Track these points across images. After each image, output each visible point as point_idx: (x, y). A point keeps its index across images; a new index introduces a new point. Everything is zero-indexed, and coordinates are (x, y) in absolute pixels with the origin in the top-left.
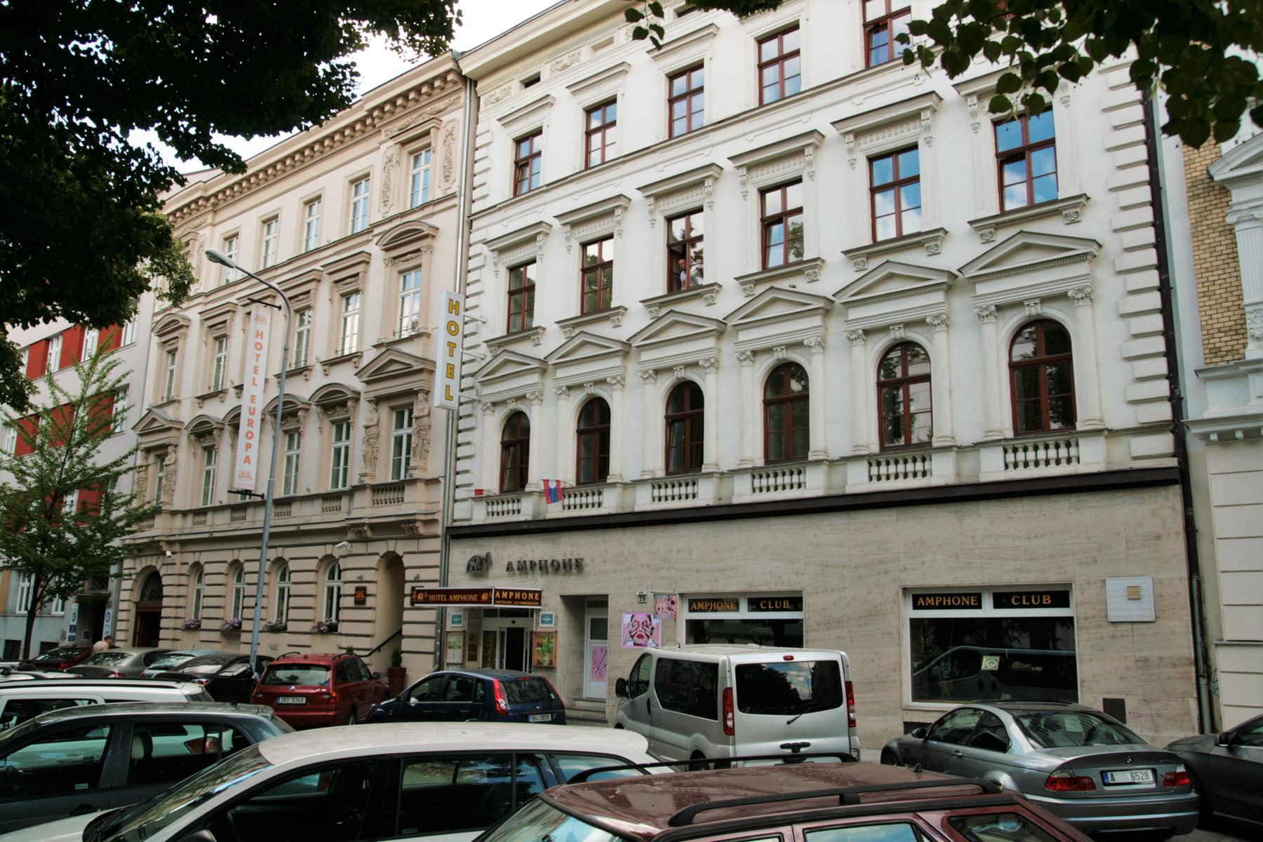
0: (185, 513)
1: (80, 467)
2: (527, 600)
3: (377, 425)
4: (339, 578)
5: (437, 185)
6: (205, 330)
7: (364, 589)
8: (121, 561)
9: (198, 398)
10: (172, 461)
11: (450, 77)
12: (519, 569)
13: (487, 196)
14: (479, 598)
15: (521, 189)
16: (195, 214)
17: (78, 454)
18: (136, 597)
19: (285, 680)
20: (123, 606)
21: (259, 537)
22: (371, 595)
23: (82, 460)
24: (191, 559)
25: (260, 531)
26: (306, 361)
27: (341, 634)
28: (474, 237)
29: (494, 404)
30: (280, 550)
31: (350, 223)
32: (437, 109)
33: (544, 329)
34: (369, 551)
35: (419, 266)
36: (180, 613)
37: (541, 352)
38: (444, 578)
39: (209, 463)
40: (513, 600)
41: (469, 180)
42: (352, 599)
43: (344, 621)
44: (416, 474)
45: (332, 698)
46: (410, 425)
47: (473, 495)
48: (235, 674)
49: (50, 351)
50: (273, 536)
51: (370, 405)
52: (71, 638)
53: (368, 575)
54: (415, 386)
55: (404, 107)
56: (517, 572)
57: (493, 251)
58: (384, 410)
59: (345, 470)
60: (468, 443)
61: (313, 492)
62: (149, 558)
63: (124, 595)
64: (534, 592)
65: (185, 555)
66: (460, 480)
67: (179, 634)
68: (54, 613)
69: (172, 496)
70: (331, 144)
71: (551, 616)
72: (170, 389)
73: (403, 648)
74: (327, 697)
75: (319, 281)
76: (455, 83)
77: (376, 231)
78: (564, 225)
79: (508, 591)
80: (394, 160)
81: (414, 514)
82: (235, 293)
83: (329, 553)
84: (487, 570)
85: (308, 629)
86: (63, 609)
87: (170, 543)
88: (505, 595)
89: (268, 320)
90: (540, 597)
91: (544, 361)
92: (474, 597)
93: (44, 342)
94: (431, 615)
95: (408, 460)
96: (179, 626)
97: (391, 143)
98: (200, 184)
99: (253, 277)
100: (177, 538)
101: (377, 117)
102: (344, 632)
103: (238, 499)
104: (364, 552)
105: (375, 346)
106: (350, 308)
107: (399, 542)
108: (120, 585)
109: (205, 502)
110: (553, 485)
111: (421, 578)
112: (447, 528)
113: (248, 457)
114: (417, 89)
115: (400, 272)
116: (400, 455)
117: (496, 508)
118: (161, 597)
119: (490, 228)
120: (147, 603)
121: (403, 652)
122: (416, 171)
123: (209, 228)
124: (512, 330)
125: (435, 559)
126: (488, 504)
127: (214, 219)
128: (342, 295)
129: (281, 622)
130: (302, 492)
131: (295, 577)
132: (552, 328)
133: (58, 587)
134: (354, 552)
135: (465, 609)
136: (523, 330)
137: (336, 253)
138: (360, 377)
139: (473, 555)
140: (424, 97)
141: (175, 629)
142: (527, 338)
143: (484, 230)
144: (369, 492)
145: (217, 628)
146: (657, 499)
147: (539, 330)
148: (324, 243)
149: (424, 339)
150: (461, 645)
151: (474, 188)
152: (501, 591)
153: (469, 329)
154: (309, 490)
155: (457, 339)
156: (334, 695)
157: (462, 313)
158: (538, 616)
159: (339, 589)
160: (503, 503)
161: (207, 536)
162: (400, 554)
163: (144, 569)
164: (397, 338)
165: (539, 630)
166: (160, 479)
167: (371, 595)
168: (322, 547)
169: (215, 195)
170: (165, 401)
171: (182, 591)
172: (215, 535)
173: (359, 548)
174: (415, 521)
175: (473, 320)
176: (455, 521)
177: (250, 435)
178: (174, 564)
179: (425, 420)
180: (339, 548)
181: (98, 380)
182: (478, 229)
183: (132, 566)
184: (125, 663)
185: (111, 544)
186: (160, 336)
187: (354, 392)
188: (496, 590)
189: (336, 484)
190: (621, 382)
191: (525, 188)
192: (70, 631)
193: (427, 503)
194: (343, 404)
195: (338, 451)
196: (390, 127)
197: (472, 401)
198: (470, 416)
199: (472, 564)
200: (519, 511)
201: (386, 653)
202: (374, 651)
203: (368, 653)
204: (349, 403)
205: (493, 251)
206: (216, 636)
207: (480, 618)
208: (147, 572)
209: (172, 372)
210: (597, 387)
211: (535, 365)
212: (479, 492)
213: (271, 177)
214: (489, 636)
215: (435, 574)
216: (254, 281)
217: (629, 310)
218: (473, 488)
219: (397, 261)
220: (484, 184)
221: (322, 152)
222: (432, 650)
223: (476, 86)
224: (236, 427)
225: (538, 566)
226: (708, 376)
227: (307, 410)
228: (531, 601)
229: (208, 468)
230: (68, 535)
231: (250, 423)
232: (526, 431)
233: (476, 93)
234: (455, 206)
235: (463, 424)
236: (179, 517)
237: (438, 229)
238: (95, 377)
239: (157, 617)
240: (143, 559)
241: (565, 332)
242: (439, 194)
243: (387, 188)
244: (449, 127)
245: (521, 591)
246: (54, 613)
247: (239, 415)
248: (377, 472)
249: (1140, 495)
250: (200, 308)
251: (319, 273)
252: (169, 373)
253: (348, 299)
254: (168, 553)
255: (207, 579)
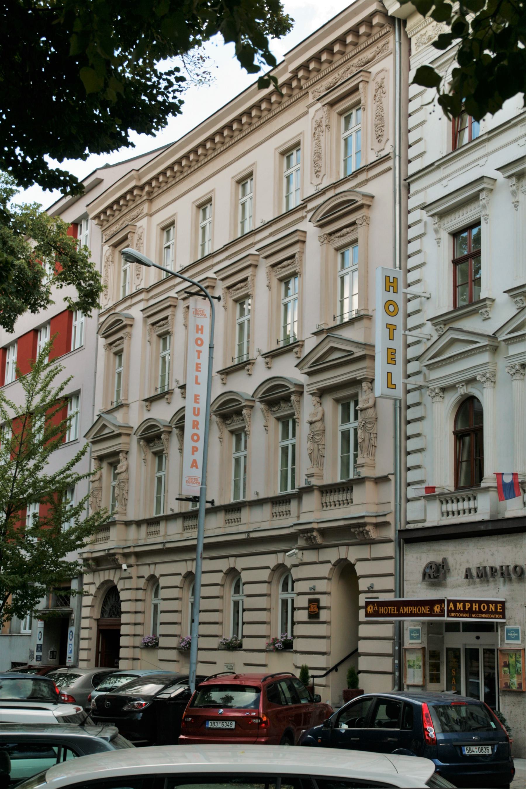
0: (139, 523)
1: (30, 480)
2: (488, 612)
3: (322, 419)
4: (293, 590)
5: (369, 148)
6: (148, 328)
7: (317, 601)
8: (80, 575)
9: (146, 400)
10: (124, 469)
11: (376, 21)
12: (478, 576)
13: (424, 153)
14: (431, 609)
15: (461, 139)
16: (132, 205)
17: (28, 467)
18: (97, 615)
19: (219, 701)
20: (85, 623)
21: (193, 549)
22: (324, 608)
23: (32, 474)
24: (146, 571)
25: (194, 542)
26: (248, 353)
27: (296, 652)
28: (413, 202)
29: (444, 390)
30: (232, 559)
31: (284, 200)
32: (364, 60)
33: (493, 300)
34: (321, 559)
35: (356, 241)
36: (139, 630)
37: (489, 328)
38: (400, 589)
39: (160, 469)
40: (471, 612)
41: (403, 137)
42: (306, 612)
43: (299, 637)
44: (364, 472)
45: (262, 722)
46: (356, 418)
47: (423, 493)
48: (173, 695)
49: (7, 360)
50: (208, 547)
51: (314, 398)
52: (39, 658)
53: (321, 586)
54: (358, 375)
55: (318, 71)
56: (478, 580)
57: (432, 216)
58: (328, 403)
59: (293, 470)
60: (418, 435)
61: (262, 496)
62: (107, 572)
63: (86, 612)
64: (496, 603)
65: (140, 568)
66: (412, 476)
67: (138, 653)
68: (23, 631)
69: (126, 505)
70: (259, 114)
71: (517, 631)
72: (118, 392)
73: (361, 667)
74: (256, 721)
75: (256, 266)
76: (382, 26)
77: (310, 206)
78: (509, 177)
79: (464, 602)
80: (324, 124)
81: (363, 517)
82: (175, 286)
83: (280, 562)
84: (445, 578)
85: (263, 647)
86: (30, 628)
87: (126, 556)
88: (460, 606)
89: (208, 311)
90: (503, 608)
91: (494, 337)
92: (426, 609)
93: (32, 333)
94: (388, 630)
95: (356, 456)
96: (137, 644)
97: (319, 105)
98: (133, 173)
99: (176, 276)
100: (131, 550)
101: (303, 77)
102: (298, 650)
103: (189, 507)
104: (368, 556)
105: (315, 334)
106: (291, 292)
107: (351, 548)
108: (81, 601)
109: (158, 510)
110: (508, 479)
111: (376, 588)
112: (400, 531)
113: (195, 462)
114: (341, 40)
115: (337, 250)
116: (348, 451)
117: (453, 507)
118: (119, 613)
119: (428, 190)
120: (109, 620)
121: (360, 672)
122: (348, 132)
123: (146, 219)
124: (460, 304)
125: (389, 566)
126: (442, 503)
127: (150, 208)
128: (281, 280)
129: (236, 639)
130: (251, 497)
131: (248, 589)
132: (502, 299)
133: (16, 605)
134: (305, 560)
135: (423, 623)
136: (471, 304)
137: (271, 235)
138: (301, 369)
139: (429, 561)
140: (325, 66)
141: (134, 647)
142: (474, 312)
143: (422, 193)
144: (316, 494)
145: (175, 645)
146: (445, 514)
147: (487, 302)
148: (258, 224)
149: (365, 322)
150: (421, 663)
151: (410, 146)
152: (455, 602)
153: (412, 307)
154: (257, 494)
155: (398, 320)
156: (265, 719)
157: (402, 289)
158: (502, 630)
159: (293, 601)
160: (458, 501)
161: (243, 536)
162: (353, 562)
163: (103, 584)
164: (338, 323)
165: (505, 647)
166: (114, 488)
167: (324, 608)
168: (274, 556)
169: (149, 183)
170: (115, 405)
171: (139, 606)
172: (168, 545)
173: (309, 556)
174: (365, 524)
175: (416, 297)
176: (408, 523)
177: (195, 438)
178: (131, 578)
179: (370, 412)
180: (290, 556)
181: (41, 390)
182: (417, 192)
183: (91, 581)
184: (75, 684)
185: (64, 559)
186: (106, 337)
187: (296, 385)
188: (449, 601)
189: (284, 486)
190: (492, 379)
191: (466, 139)
192: (38, 650)
193: (378, 504)
194: (286, 399)
195: (285, 450)
196: (317, 87)
197: (420, 388)
198: (418, 404)
199: (428, 571)
200: (476, 510)
201: (342, 675)
202: (331, 670)
203: (324, 672)
204: (293, 398)
205: (432, 216)
206: (173, 655)
207: (441, 634)
208: (105, 587)
209: (119, 374)
210: (469, 386)
211: (484, 342)
212: (430, 489)
213: (202, 157)
214: (454, 653)
215: (389, 583)
216: (179, 280)
217: (497, 301)
218: (424, 486)
219: (333, 237)
220: (420, 140)
221: (250, 124)
222: (390, 670)
223: (405, 26)
224: (182, 429)
225: (499, 573)
226: (485, 391)
227: (252, 407)
228: (492, 613)
229: (159, 474)
230: (23, 552)
231: (195, 425)
232: (479, 415)
233: (406, 33)
234: (390, 169)
235: (411, 414)
236: (133, 527)
237: (373, 197)
238: (39, 386)
239: (117, 635)
240: (102, 573)
241: (516, 302)
242: (372, 158)
243: (318, 156)
244: (378, 79)
245: (480, 602)
246: (23, 631)
247: (183, 418)
248: (324, 472)
249: (515, 537)
250: (142, 306)
251: (256, 258)
252: (117, 375)
253: (287, 284)
254: (124, 567)
255: (248, 589)
